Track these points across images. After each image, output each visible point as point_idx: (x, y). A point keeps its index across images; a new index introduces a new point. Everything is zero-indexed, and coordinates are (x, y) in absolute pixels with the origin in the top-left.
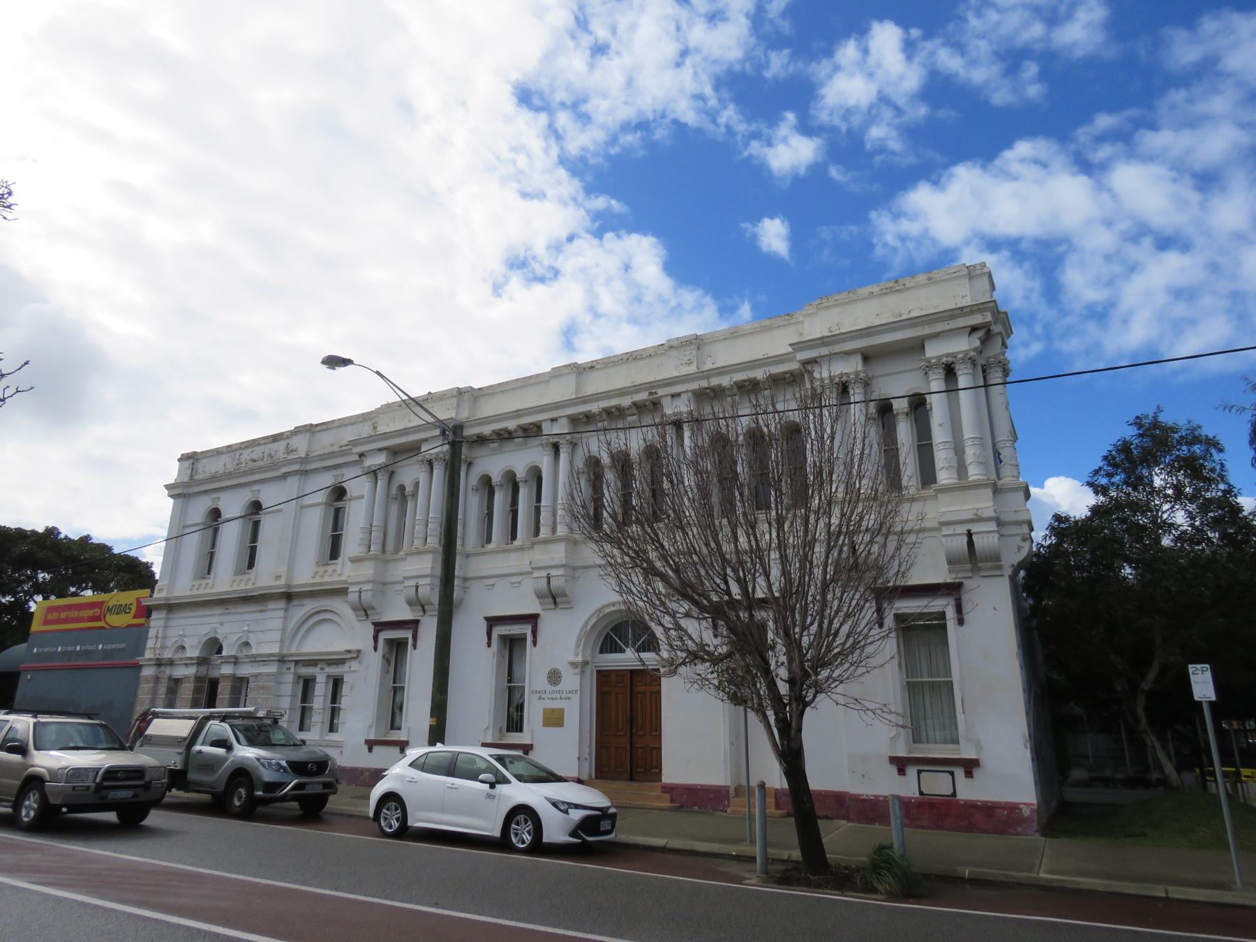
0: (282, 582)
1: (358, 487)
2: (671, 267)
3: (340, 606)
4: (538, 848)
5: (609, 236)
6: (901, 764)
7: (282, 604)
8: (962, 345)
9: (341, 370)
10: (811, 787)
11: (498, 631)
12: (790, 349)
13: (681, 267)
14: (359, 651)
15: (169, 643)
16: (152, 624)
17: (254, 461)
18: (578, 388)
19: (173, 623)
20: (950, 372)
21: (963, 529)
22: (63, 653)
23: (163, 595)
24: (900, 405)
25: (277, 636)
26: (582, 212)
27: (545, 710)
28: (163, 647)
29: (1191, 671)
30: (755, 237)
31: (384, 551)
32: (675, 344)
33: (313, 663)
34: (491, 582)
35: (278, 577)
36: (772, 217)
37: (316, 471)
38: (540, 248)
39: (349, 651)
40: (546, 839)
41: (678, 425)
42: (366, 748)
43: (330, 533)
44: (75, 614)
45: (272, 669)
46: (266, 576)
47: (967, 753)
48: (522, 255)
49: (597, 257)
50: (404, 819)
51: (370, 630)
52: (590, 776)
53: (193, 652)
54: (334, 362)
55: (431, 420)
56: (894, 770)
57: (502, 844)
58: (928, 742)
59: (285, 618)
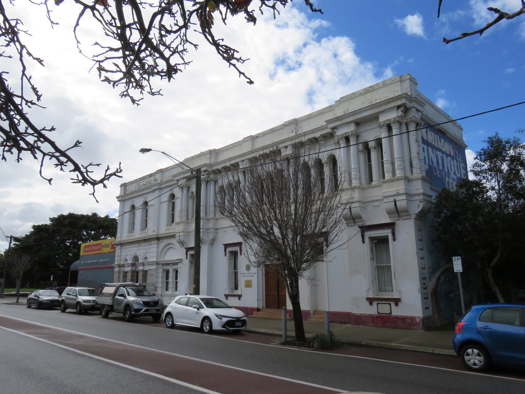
0: (155, 233)
1: (177, 192)
2: (357, 52)
3: (174, 241)
4: (212, 332)
5: (324, 40)
6: (371, 301)
7: (156, 242)
8: (393, 115)
9: (147, 154)
10: (302, 309)
11: (229, 249)
12: (325, 124)
13: (362, 52)
14: (181, 259)
15: (122, 258)
16: (117, 251)
17: (144, 185)
18: (252, 147)
19: (123, 250)
20: (389, 128)
21: (392, 199)
22: (91, 263)
23: (119, 240)
24: (372, 144)
25: (155, 254)
26: (308, 30)
27: (245, 281)
28: (121, 260)
29: (453, 259)
30: (404, 26)
31: (188, 219)
32: (287, 124)
33: (168, 264)
34: (225, 230)
35: (154, 231)
36: (413, 15)
37: (164, 188)
38: (290, 52)
39: (178, 260)
40: (213, 328)
41: (288, 160)
43: (171, 213)
44: (93, 248)
45: (154, 267)
46: (150, 232)
47: (396, 296)
48: (281, 58)
49: (320, 52)
50: (173, 322)
51: (185, 251)
52: (263, 307)
53: (130, 262)
54: (144, 151)
55: (189, 169)
56: (368, 303)
57: (200, 330)
58: (386, 291)
59: (158, 247)
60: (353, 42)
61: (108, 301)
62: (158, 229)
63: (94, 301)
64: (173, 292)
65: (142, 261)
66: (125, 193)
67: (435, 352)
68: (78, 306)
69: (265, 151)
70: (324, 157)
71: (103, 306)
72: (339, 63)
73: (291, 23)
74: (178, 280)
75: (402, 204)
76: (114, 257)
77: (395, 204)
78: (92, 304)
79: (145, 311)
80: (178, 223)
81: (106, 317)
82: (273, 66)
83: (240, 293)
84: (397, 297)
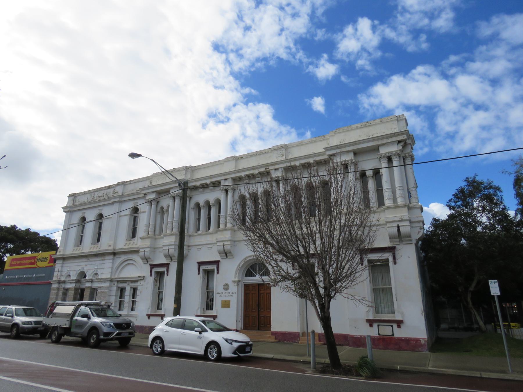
0: (112, 248)
1: (144, 208)
2: (276, 117)
4: (220, 359)
6: (371, 322)
8: (395, 148)
10: (334, 332)
11: (203, 268)
13: (280, 116)
14: (144, 277)
15: (64, 273)
16: (56, 266)
17: (100, 197)
18: (236, 167)
19: (65, 265)
20: (390, 159)
21: (395, 224)
23: (61, 253)
24: (369, 173)
25: (109, 270)
26: (239, 94)
27: (222, 301)
28: (61, 276)
30: (311, 105)
33: (124, 282)
34: (200, 247)
35: (110, 246)
36: (317, 97)
37: (126, 201)
39: (140, 277)
41: (277, 181)
42: (147, 317)
43: (132, 227)
44: (23, 262)
45: (107, 284)
46: (105, 245)
47: (398, 318)
50: (163, 347)
51: (149, 268)
53: (74, 278)
56: (368, 325)
57: (204, 357)
59: (113, 263)
60: (273, 108)
61: (64, 323)
62: (115, 243)
63: (36, 323)
64: (128, 312)
65: (91, 278)
66: (73, 203)
67: (484, 376)
68: (15, 329)
69: (293, 164)
70: (315, 182)
71: (55, 328)
72: (259, 123)
73: (227, 86)
74: (138, 298)
75: (405, 229)
76: (53, 272)
77: (399, 230)
78: (33, 325)
79: (117, 334)
80: (142, 238)
81: (57, 341)
82: (205, 117)
83: (163, 313)
84: (400, 318)
